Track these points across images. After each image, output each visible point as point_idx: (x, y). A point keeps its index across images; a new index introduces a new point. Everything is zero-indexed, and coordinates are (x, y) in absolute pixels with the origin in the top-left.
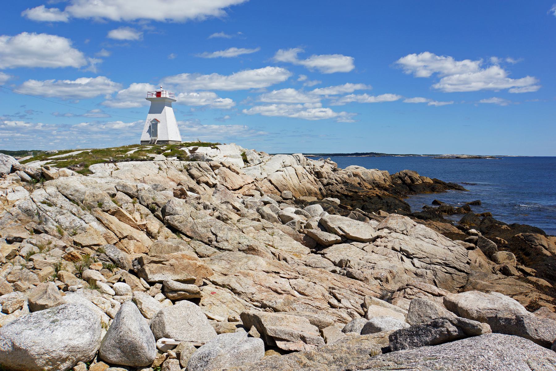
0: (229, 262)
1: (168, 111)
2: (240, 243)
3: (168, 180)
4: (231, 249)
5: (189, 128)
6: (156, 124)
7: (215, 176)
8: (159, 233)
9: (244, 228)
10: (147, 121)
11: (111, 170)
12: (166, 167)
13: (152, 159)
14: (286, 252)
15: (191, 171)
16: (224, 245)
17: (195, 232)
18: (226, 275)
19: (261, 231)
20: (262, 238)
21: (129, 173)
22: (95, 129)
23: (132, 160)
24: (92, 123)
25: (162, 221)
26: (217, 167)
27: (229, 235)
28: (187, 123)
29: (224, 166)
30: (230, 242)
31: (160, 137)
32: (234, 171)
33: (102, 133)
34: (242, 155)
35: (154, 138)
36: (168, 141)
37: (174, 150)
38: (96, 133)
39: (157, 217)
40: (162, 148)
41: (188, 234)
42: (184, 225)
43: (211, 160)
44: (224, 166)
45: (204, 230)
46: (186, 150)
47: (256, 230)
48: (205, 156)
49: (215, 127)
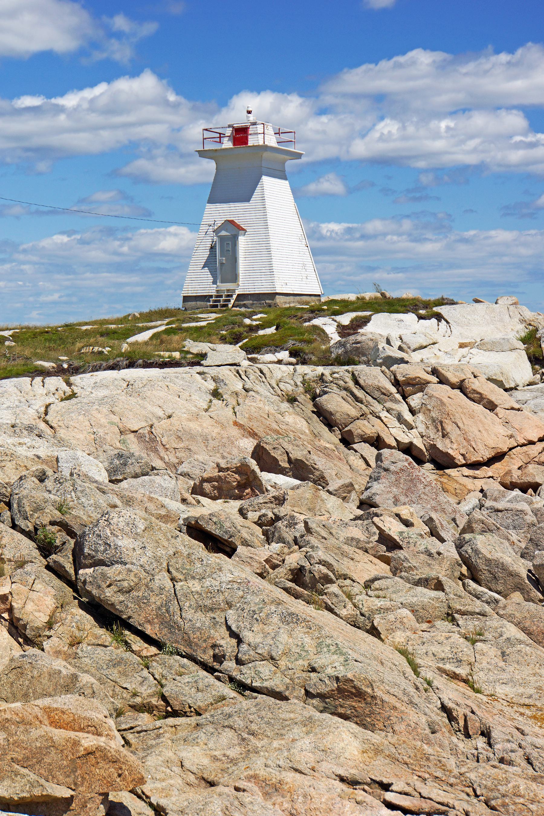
0: (246, 736)
1: (275, 192)
2: (313, 670)
3: (235, 432)
4: (280, 688)
5: (413, 245)
6: (234, 239)
7: (408, 416)
8: (50, 625)
9: (380, 610)
10: (203, 228)
11: (51, 399)
12: (238, 386)
13: (198, 360)
14: (511, 704)
15: (323, 400)
16: (258, 673)
17: (171, 626)
18: (212, 784)
19: (439, 623)
20: (435, 648)
21: (105, 410)
22: (95, 254)
23: (131, 365)
24: (87, 236)
25: (72, 584)
26: (420, 386)
27: (284, 637)
28: (407, 225)
29: (443, 381)
30: (283, 663)
31: (246, 284)
32: (478, 398)
33: (118, 267)
34: (524, 341)
35: (225, 286)
36: (273, 295)
37: (273, 326)
38: (95, 267)
39: (56, 570)
40: (247, 321)
41: (149, 630)
42: (138, 601)
43: (402, 361)
44: (443, 381)
45: (201, 619)
46: (329, 326)
47: (420, 619)
48: (382, 345)
49: (502, 236)
